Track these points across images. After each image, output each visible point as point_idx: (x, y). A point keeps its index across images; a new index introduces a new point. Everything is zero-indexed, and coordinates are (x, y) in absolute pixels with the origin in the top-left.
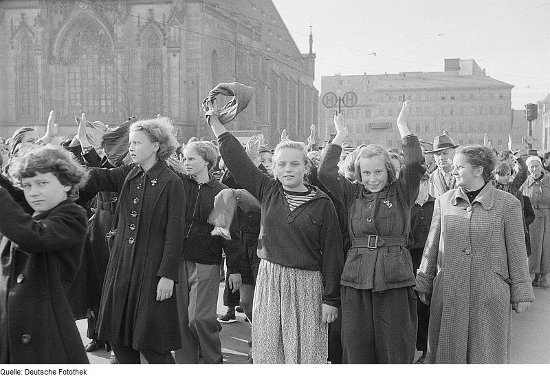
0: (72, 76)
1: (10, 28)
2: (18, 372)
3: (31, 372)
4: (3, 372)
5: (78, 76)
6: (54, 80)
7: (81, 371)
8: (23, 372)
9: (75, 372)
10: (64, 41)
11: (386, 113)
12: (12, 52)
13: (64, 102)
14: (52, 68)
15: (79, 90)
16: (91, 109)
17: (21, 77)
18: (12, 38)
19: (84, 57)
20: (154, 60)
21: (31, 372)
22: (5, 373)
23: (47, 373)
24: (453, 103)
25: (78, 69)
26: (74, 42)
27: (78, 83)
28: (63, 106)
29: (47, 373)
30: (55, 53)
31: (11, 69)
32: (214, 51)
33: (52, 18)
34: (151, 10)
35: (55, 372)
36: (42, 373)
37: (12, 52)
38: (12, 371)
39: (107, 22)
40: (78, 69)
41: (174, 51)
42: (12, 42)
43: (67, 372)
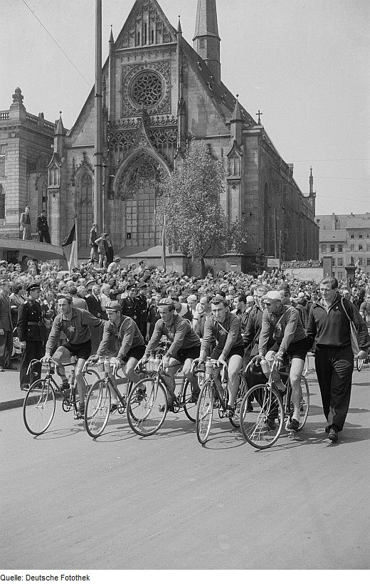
0: (129, 210)
1: (71, 167)
2: (18, 578)
3: (33, 578)
4: (3, 577)
5: (135, 209)
6: (112, 213)
7: (84, 577)
8: (24, 578)
9: (77, 578)
10: (123, 177)
11: (357, 248)
12: (73, 189)
13: (121, 234)
14: (111, 203)
15: (135, 223)
16: (147, 241)
17: (80, 213)
18: (73, 176)
19: (141, 191)
20: (87, 198)
21: (33, 578)
22: (5, 579)
23: (48, 578)
24: (360, 253)
25: (135, 203)
26: (132, 178)
27: (135, 216)
28: (121, 239)
29: (48, 578)
30: (114, 188)
31: (72, 205)
32: (266, 184)
33: (112, 156)
34: (209, 145)
35: (56, 577)
36: (44, 578)
37: (73, 189)
38: (12, 577)
39: (166, 159)
40: (135, 203)
41: (234, 183)
42: (73, 180)
43: (69, 578)
